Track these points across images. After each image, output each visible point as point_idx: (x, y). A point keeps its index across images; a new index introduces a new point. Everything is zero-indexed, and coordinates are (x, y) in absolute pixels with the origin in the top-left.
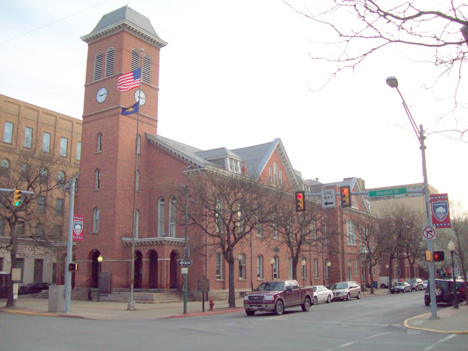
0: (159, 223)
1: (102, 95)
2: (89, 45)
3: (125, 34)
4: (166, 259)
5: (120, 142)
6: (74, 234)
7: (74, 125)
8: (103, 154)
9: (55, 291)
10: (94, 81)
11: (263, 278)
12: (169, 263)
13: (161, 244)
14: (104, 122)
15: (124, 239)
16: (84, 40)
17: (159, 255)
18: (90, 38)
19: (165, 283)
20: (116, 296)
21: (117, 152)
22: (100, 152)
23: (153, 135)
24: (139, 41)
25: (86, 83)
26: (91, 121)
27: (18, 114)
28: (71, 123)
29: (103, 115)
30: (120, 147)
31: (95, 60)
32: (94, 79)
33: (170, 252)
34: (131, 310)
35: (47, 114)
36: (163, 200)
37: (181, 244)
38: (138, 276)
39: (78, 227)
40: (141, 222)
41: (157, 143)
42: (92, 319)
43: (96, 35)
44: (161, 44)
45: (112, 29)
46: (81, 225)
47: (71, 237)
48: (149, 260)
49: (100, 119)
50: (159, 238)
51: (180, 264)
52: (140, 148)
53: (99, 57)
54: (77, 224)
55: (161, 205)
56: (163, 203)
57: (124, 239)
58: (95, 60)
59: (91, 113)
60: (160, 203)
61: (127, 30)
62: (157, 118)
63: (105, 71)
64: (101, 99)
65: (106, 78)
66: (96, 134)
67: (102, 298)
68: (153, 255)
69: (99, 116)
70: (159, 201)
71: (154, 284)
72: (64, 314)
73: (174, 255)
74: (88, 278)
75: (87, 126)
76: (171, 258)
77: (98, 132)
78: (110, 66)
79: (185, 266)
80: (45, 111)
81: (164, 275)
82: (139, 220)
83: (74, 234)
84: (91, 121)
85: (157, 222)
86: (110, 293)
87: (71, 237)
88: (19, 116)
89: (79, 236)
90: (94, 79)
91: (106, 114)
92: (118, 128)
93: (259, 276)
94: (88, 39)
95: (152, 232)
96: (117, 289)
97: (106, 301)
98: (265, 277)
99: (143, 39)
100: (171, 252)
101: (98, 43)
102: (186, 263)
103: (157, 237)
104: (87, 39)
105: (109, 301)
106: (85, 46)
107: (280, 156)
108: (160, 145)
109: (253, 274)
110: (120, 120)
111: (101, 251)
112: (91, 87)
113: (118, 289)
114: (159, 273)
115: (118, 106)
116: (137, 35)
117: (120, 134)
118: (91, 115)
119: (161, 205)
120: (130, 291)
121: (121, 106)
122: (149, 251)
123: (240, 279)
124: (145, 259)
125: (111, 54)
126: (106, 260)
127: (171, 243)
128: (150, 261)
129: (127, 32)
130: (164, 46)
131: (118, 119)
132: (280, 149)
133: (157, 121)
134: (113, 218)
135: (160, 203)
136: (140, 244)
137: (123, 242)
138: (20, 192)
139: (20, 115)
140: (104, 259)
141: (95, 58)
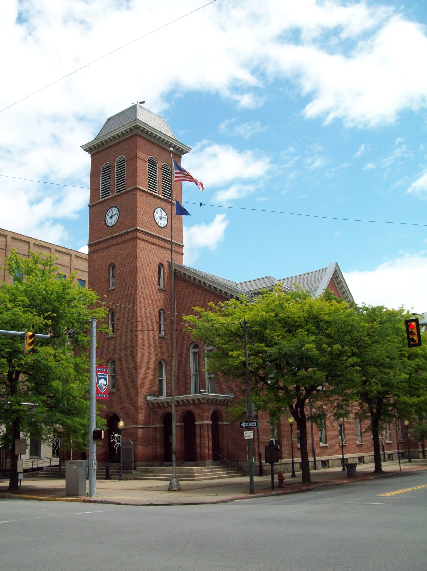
0: (192, 378)
1: (112, 217)
2: (92, 156)
3: (139, 139)
4: (206, 422)
5: (139, 275)
6: (98, 391)
7: (72, 259)
8: (117, 290)
9: (74, 467)
10: (101, 200)
11: (326, 443)
12: (210, 427)
13: (198, 403)
14: (117, 250)
15: (149, 398)
16: (86, 150)
17: (197, 418)
18: (94, 146)
19: (207, 453)
20: (142, 472)
21: (135, 287)
22: (114, 288)
23: (178, 264)
24: (156, 148)
25: (90, 203)
26: (100, 249)
27: (4, 248)
28: (68, 258)
29: (114, 242)
30: (139, 280)
31: (101, 173)
32: (101, 197)
33: (211, 412)
34: (175, 491)
35: (40, 246)
36: (196, 346)
37: (224, 402)
38: (168, 445)
39: (102, 382)
40: (169, 376)
41: (185, 274)
42: (132, 505)
43: (101, 142)
44: (183, 150)
45: (122, 133)
46: (105, 379)
47: (94, 395)
48: (163, 425)
49: (111, 246)
50: (193, 395)
51: (242, 427)
52: (164, 281)
53: (105, 169)
54: (101, 378)
55: (195, 353)
56: (196, 350)
57: (149, 398)
58: (101, 173)
59: (100, 240)
60: (192, 350)
61: (140, 133)
62: (182, 243)
63: (115, 186)
64: (110, 222)
65: (116, 194)
66: (107, 265)
67: (124, 475)
68: (189, 419)
69: (110, 243)
70: (191, 348)
71: (190, 456)
72: (88, 498)
73: (216, 417)
74: (104, 450)
75: (95, 256)
76: (164, 424)
77: (109, 263)
78: (121, 178)
79: (249, 429)
80: (37, 242)
81: (206, 444)
82: (166, 374)
83: (98, 391)
84: (100, 249)
85: (189, 376)
86: (135, 469)
87: (94, 395)
88: (6, 250)
89: (104, 393)
90: (101, 197)
91: (119, 240)
92: (136, 257)
93: (321, 440)
94: (90, 148)
95: (183, 388)
96: (142, 463)
97: (130, 479)
98: (328, 442)
99: (160, 144)
100: (212, 412)
101: (103, 153)
102: (250, 424)
103: (191, 394)
104: (90, 148)
105: (135, 479)
106: (87, 158)
107: (337, 285)
108: (189, 276)
109: (315, 438)
110: (138, 247)
111: (120, 415)
112: (96, 208)
113: (144, 463)
114: (198, 441)
115: (134, 228)
116: (152, 140)
117: (138, 264)
118: (99, 242)
119: (195, 353)
120: (171, 465)
121: (138, 228)
122: (163, 414)
123: (321, 444)
124: (175, 424)
125: (122, 164)
126: (130, 426)
127: (210, 401)
128: (184, 426)
129: (141, 137)
130: (187, 152)
131: (135, 246)
132: (337, 278)
133: (182, 246)
134: (135, 371)
135: (192, 350)
136: (181, 403)
137: (148, 402)
138: (33, 336)
139: (8, 248)
140: (125, 424)
141: (101, 171)
